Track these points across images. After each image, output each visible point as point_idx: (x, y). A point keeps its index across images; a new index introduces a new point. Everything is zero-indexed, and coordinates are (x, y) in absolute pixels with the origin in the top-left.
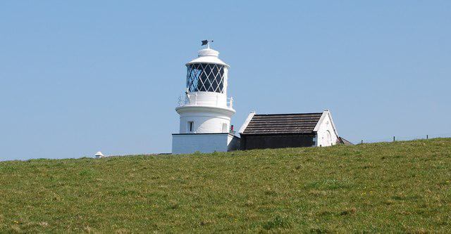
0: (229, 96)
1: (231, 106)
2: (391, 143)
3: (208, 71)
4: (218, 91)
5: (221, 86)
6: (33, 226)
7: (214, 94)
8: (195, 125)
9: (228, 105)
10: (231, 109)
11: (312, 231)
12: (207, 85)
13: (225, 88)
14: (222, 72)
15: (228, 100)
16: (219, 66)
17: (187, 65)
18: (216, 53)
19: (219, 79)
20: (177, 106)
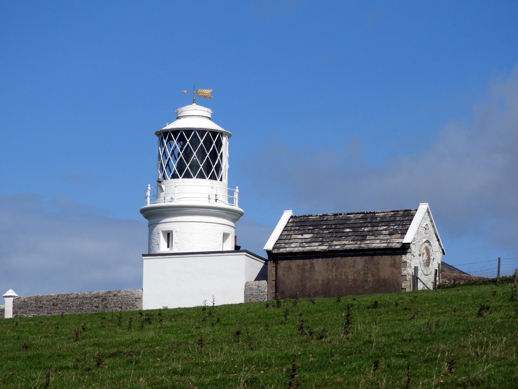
0: (231, 185)
1: (236, 202)
2: (211, 307)
3: (195, 142)
4: (213, 177)
5: (218, 168)
6: (13, 359)
7: (207, 182)
8: (175, 237)
9: (231, 201)
10: (236, 207)
11: (437, 386)
12: (194, 167)
13: (225, 165)
14: (219, 144)
15: (231, 193)
16: (214, 133)
17: (158, 134)
18: (206, 112)
19: (214, 155)
20: (156, 131)
